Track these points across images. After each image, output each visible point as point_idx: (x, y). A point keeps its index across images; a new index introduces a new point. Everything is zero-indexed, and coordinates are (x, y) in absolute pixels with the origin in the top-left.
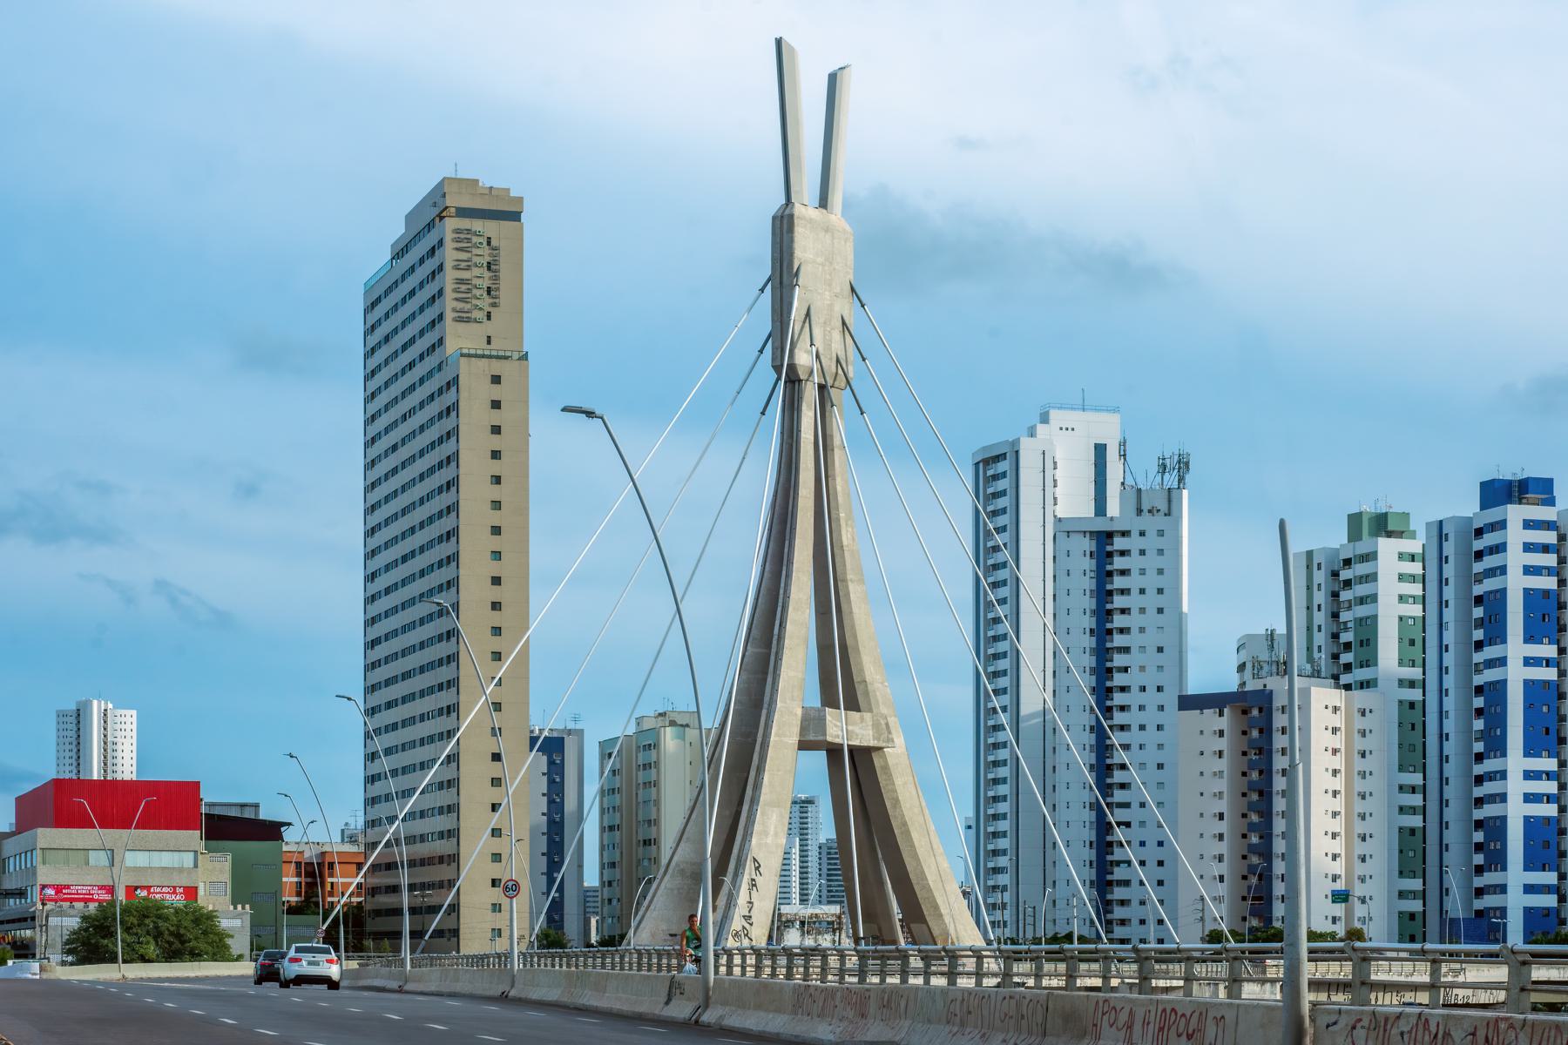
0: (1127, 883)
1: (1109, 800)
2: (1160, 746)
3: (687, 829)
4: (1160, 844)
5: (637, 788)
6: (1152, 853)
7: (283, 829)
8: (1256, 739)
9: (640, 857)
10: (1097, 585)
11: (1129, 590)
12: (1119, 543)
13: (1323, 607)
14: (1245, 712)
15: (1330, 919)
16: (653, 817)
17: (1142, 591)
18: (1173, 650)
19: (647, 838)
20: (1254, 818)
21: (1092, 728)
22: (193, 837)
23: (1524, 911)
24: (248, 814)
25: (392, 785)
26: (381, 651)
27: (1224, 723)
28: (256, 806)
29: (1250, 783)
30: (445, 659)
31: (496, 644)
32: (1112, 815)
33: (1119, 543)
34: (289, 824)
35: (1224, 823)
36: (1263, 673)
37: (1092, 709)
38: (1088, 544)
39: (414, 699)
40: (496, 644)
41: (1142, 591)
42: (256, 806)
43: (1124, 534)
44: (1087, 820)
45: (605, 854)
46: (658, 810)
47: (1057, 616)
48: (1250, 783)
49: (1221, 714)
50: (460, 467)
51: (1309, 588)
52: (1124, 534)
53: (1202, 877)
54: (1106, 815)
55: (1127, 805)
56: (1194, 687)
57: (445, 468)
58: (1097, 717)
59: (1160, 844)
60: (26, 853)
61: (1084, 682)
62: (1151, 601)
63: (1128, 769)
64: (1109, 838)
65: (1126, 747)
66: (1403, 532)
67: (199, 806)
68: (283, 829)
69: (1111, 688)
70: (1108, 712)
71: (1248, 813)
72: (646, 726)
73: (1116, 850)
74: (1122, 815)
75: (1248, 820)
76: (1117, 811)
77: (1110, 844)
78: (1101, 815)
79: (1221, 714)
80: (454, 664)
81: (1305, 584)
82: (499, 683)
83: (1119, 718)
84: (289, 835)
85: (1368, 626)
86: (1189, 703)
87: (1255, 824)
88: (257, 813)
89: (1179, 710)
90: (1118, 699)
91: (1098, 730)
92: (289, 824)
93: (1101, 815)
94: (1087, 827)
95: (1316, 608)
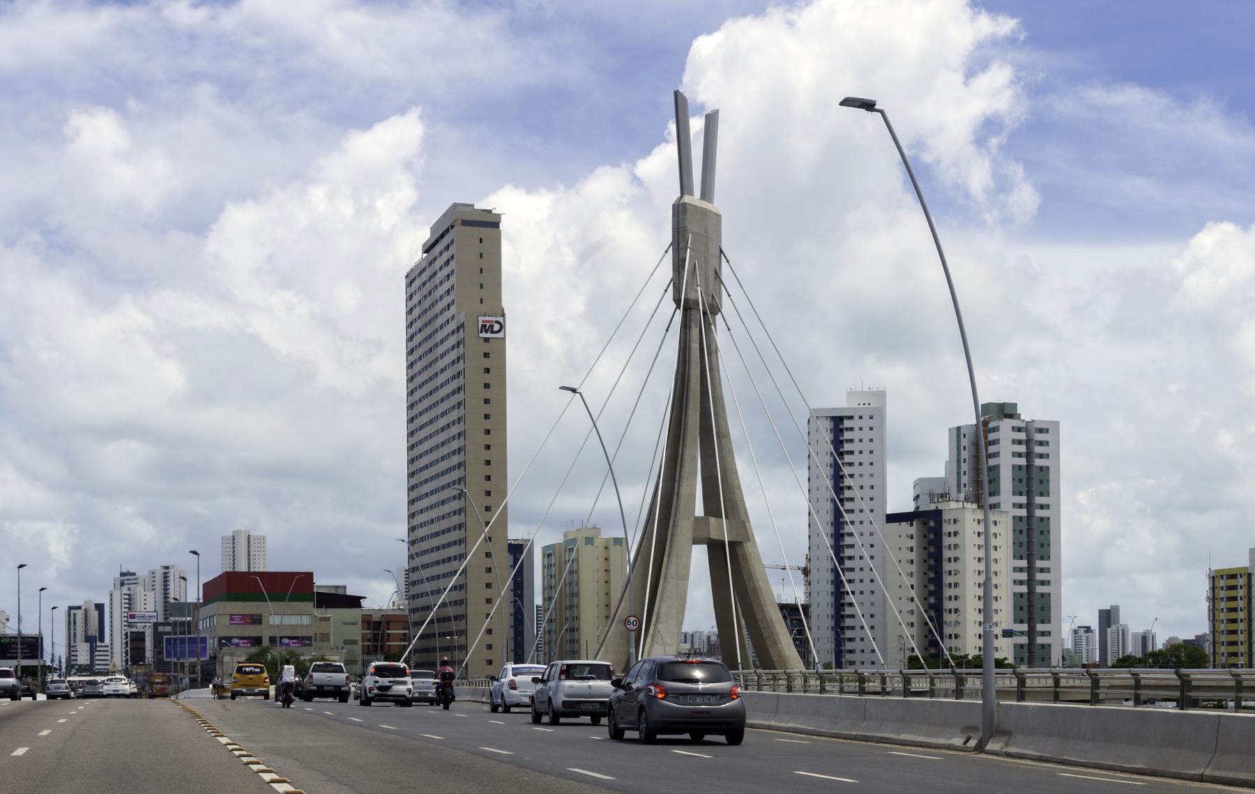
0: (852, 628)
1: (842, 567)
2: (872, 475)
3: (595, 360)
4: (872, 581)
5: (565, 552)
6: (868, 540)
7: (361, 601)
8: (933, 539)
9: (567, 616)
10: (834, 426)
11: (853, 463)
12: (847, 423)
13: (967, 473)
14: (925, 524)
15: (977, 572)
16: (576, 591)
17: (861, 581)
18: (877, 489)
19: (572, 633)
20: (932, 587)
21: (832, 570)
22: (309, 606)
23: (1100, 616)
24: (340, 592)
25: (427, 587)
26: (419, 561)
27: (913, 530)
28: (345, 587)
29: (929, 592)
30: (457, 496)
31: (488, 501)
32: (844, 575)
33: (847, 423)
34: (365, 598)
35: (914, 553)
36: (936, 500)
37: (832, 453)
38: (829, 425)
39: (438, 448)
40: (488, 501)
41: (861, 429)
42: (345, 587)
43: (851, 418)
44: (829, 579)
45: (546, 592)
46: (578, 599)
47: (811, 549)
48: (929, 592)
49: (912, 525)
50: (468, 593)
51: (959, 473)
52: (851, 418)
53: (900, 611)
54: (840, 576)
55: (852, 570)
56: (891, 509)
57: (456, 409)
58: (835, 564)
59: (872, 581)
60: (214, 638)
61: (828, 542)
62: (867, 493)
63: (852, 489)
64: (842, 590)
65: (851, 476)
66: (1013, 415)
67: (313, 587)
68: (361, 601)
69: (844, 627)
70: (841, 454)
71: (928, 585)
72: (570, 537)
73: (846, 596)
74: (849, 575)
75: (928, 576)
76: (846, 573)
77: (843, 593)
78: (836, 507)
79: (912, 525)
80: (463, 591)
81: (956, 471)
82: (488, 615)
83: (848, 564)
84: (364, 603)
85: (995, 470)
86: (892, 518)
87: (933, 591)
88: (345, 591)
89: (887, 522)
90: (847, 447)
91: (834, 570)
92: (365, 598)
93: (836, 507)
94: (830, 606)
95: (962, 473)
